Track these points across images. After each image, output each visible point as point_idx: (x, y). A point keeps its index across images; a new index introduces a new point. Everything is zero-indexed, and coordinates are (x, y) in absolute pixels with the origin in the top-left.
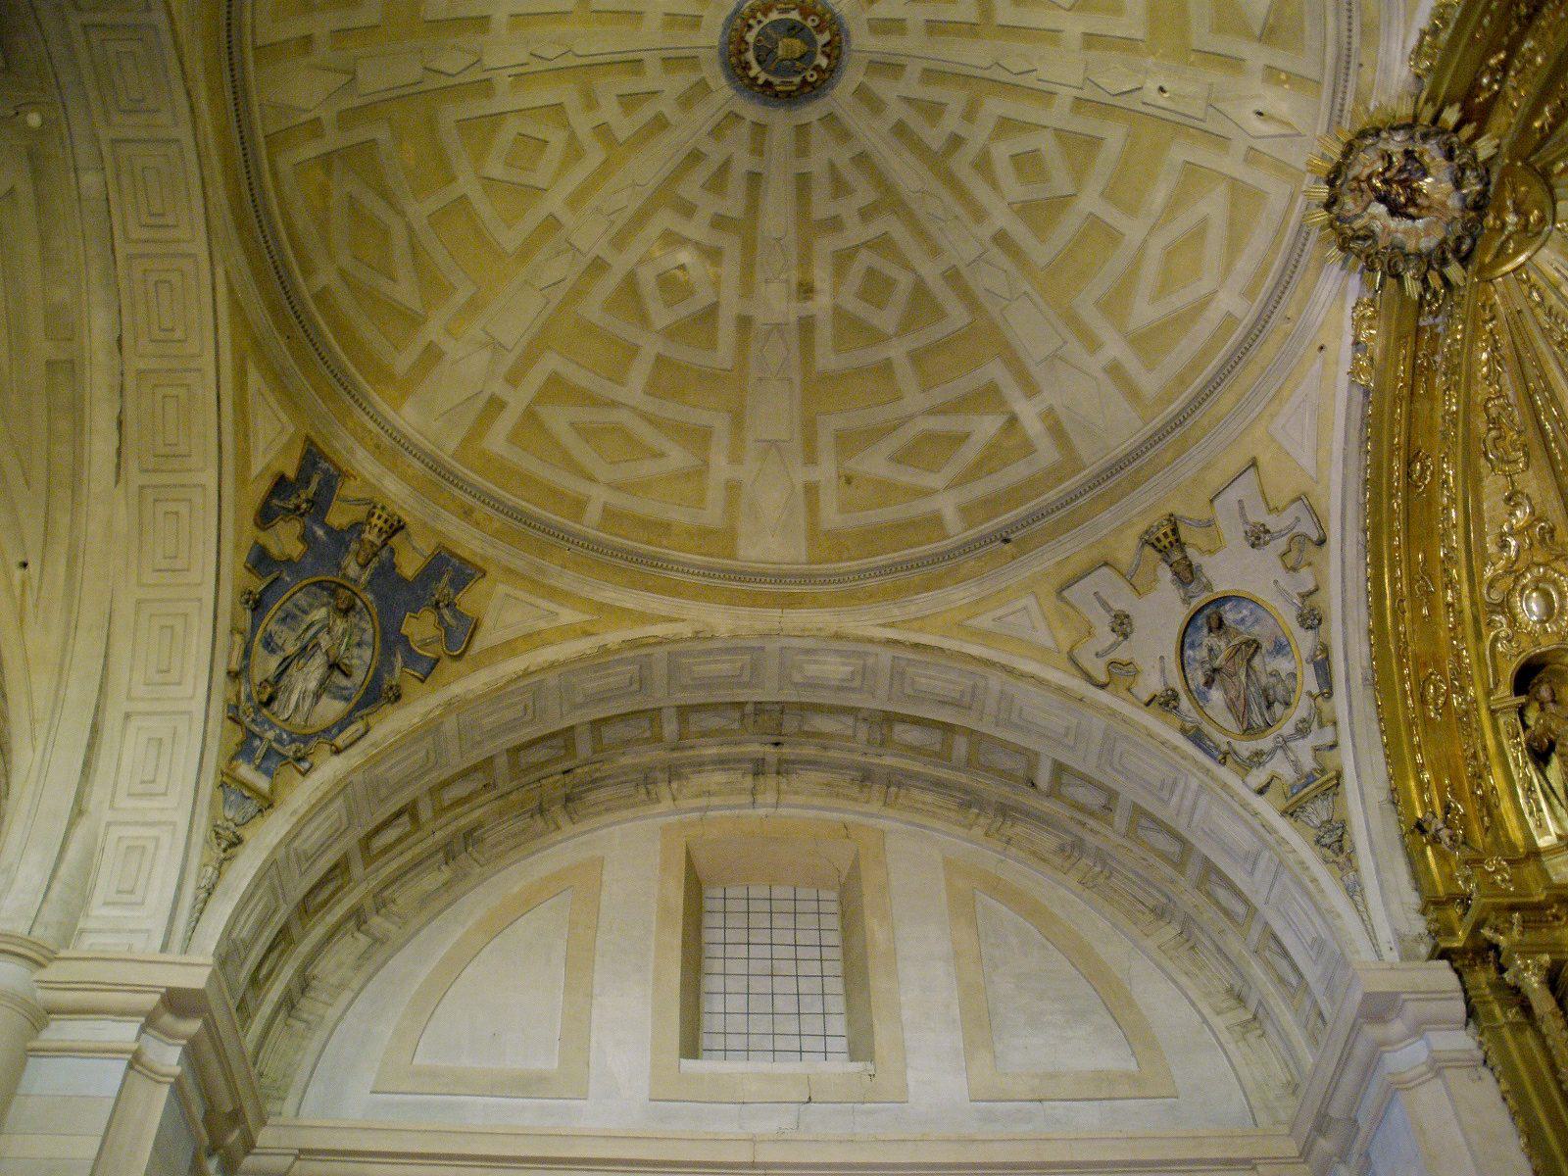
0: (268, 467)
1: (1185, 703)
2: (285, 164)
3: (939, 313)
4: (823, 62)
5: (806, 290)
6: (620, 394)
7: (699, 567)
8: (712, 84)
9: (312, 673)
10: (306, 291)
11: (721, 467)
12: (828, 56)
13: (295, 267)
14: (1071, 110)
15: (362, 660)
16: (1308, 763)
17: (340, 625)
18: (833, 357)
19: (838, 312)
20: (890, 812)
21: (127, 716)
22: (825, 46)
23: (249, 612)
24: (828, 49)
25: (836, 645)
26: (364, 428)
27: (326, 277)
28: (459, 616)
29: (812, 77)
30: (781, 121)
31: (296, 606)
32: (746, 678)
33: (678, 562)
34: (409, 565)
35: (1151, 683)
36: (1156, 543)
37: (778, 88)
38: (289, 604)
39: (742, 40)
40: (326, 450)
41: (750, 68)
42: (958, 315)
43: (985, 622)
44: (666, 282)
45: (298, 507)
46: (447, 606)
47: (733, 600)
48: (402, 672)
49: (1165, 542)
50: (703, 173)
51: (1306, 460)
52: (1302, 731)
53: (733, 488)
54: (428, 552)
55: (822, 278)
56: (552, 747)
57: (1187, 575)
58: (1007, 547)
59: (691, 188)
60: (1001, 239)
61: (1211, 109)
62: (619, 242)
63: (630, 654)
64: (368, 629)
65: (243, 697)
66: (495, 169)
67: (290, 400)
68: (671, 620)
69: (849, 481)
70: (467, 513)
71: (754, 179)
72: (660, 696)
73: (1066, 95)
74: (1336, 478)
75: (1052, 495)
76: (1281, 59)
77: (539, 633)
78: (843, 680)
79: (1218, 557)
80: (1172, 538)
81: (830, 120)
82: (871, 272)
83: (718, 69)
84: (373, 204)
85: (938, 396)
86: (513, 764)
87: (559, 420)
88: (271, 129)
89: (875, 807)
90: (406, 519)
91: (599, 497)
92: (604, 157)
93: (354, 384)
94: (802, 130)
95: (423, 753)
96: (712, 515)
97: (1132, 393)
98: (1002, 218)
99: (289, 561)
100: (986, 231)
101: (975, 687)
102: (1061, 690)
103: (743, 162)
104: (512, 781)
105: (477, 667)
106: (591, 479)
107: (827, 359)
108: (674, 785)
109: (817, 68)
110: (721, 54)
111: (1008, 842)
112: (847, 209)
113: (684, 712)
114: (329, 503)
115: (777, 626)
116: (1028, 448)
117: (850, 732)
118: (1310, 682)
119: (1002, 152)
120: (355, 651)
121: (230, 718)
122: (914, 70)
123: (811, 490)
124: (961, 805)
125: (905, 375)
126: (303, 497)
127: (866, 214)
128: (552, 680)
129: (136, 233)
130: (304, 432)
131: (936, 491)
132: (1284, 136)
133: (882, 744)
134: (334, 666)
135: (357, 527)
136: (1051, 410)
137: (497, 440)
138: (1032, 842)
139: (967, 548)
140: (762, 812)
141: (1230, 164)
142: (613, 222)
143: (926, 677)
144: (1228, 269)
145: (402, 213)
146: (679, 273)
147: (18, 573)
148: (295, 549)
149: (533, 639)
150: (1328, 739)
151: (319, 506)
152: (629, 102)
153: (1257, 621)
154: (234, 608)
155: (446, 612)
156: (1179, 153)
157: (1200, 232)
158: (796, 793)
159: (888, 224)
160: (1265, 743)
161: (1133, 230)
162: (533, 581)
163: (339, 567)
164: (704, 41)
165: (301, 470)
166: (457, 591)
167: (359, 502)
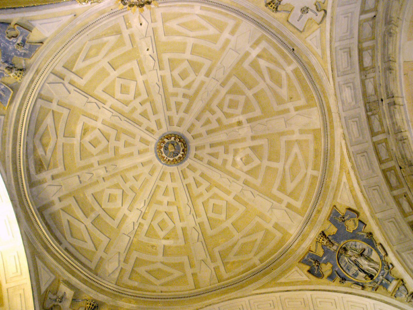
0: (306, 275)
2: (226, 276)
3: (235, 85)
4: (173, 139)
5: (240, 123)
6: (281, 169)
7: (325, 139)
8: (188, 164)
9: (364, 263)
11: (296, 136)
12: (171, 137)
13: (253, 270)
14: (164, 70)
15: (361, 245)
17: (349, 253)
18: (257, 111)
19: (243, 113)
20: (397, 60)
22: (168, 139)
23: (346, 282)
24: (169, 138)
25: (338, 95)
27: (256, 260)
29: (178, 140)
30: (193, 144)
31: (345, 266)
32: (357, 119)
33: (325, 146)
34: (333, 230)
36: (275, 8)
37: (184, 148)
38: (344, 268)
39: (173, 161)
40: (302, 256)
41: (180, 157)
43: (319, 51)
44: (246, 163)
45: (318, 266)
46: (344, 218)
47: (332, 127)
48: (363, 232)
49: (274, 6)
50: (213, 160)
53: (301, 132)
54: (330, 223)
55: (234, 120)
56: (390, 176)
58: (295, 49)
59: (219, 162)
60: (207, 75)
61: (147, 36)
62: (237, 178)
63: (353, 158)
64: (351, 243)
66: (223, 217)
67: (289, 268)
68: (341, 147)
69: (291, 98)
70: (319, 212)
71: (212, 146)
72: (369, 146)
73: (160, 73)
75: (275, 41)
76: (123, 26)
77: (350, 188)
78: (351, 89)
80: (272, 4)
81: (189, 131)
82: (229, 107)
83: (183, 164)
84: (236, 248)
85: (258, 78)
86: (396, 188)
87: (290, 186)
89: (396, 65)
90: (320, 232)
91: (310, 172)
92: (215, 187)
94: (194, 137)
95: (389, 224)
96: (310, 137)
97: (236, 26)
98: (201, 77)
99: (332, 268)
100: (207, 79)
101: (341, 49)
102: (331, 24)
103: (208, 150)
104: (404, 187)
105: (361, 207)
106: (306, 174)
107: (258, 112)
108: (402, 130)
109: (175, 139)
110: (178, 165)
111: (398, 18)
112: (213, 118)
113: (373, 134)
114: (316, 255)
115: (337, 114)
116: (264, 50)
117: (372, 80)
119: (182, 83)
120: (358, 247)
121: (376, 290)
122: (169, 114)
123: (297, 109)
124: (391, 36)
125: (256, 90)
126: (314, 264)
127: (213, 113)
128: (363, 183)
130: (298, 264)
131: (286, 73)
132: (143, 17)
133: (374, 68)
134: (361, 255)
135: (323, 247)
136: (251, 47)
137: (298, 204)
138: (397, 11)
139: (299, 61)
140: (405, 102)
141: (159, 25)
142: (233, 181)
143: (342, 64)
144: (187, 14)
145: (238, 240)
146: (243, 159)
148: (329, 265)
149: (352, 190)
151: (317, 260)
152: (198, 185)
154: (344, 286)
156: (163, 38)
158: (397, 91)
159: (214, 106)
161: (190, 42)
162: (336, 190)
163: (334, 252)
166: (340, 215)
167: (316, 246)
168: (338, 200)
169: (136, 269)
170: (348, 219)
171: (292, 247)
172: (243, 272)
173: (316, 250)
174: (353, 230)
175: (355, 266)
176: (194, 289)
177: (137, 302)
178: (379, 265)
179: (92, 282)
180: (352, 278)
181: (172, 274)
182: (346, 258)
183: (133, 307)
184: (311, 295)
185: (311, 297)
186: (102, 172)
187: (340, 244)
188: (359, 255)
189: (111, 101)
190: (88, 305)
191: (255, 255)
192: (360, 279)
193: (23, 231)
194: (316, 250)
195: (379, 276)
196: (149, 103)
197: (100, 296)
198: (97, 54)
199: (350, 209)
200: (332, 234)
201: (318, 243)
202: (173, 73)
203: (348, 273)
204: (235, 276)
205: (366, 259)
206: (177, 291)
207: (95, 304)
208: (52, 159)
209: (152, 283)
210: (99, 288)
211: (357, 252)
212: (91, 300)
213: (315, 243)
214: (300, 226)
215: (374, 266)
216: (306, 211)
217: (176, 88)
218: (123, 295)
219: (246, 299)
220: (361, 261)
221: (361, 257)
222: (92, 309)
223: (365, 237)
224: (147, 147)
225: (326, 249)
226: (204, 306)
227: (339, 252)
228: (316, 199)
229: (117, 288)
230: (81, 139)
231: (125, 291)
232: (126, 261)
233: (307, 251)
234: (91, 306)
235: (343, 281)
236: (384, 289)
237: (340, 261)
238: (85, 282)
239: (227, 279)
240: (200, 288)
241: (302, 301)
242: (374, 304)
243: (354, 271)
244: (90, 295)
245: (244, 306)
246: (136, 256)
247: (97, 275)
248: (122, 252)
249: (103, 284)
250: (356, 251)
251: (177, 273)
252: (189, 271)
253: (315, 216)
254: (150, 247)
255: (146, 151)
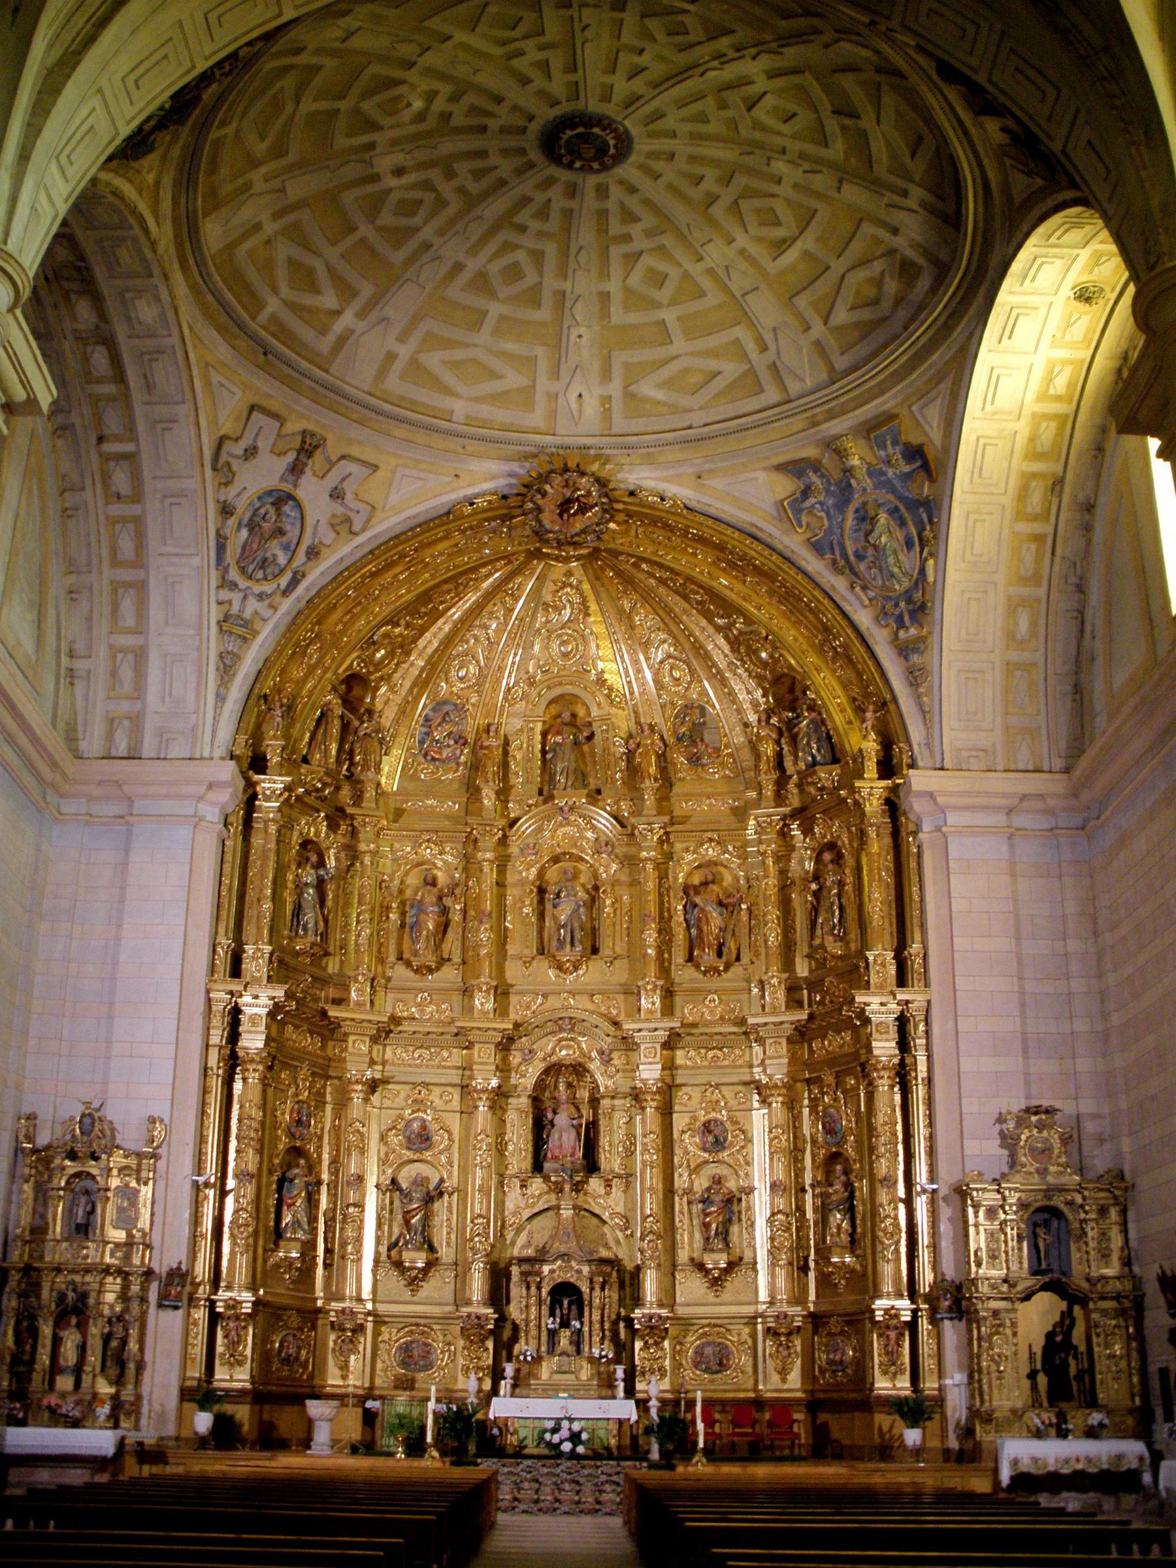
1: (232, 522)
16: (247, 614)
35: (230, 494)
42: (398, 257)
43: (215, 377)
51: (393, 498)
52: (261, 597)
55: (411, 178)
57: (296, 469)
58: (262, 357)
74: (394, 520)
76: (617, 405)
79: (314, 479)
116: (324, 331)
118: (284, 581)
119: (521, 256)
123: (257, 227)
126: (397, 630)
127: (462, 191)
141: (543, 384)
144: (477, 400)
150: (266, 616)
153: (293, 524)
157: (495, 375)
160: (243, 583)
161: (484, 336)
164: (591, 102)
186: (780, 166)
189: (696, 270)
193: (1011, 250)
196: (611, 233)
198: (686, 370)
202: (537, 279)
208: (878, 254)
217: (538, 247)
224: (649, 162)
230: (795, 240)
255: (651, 155)
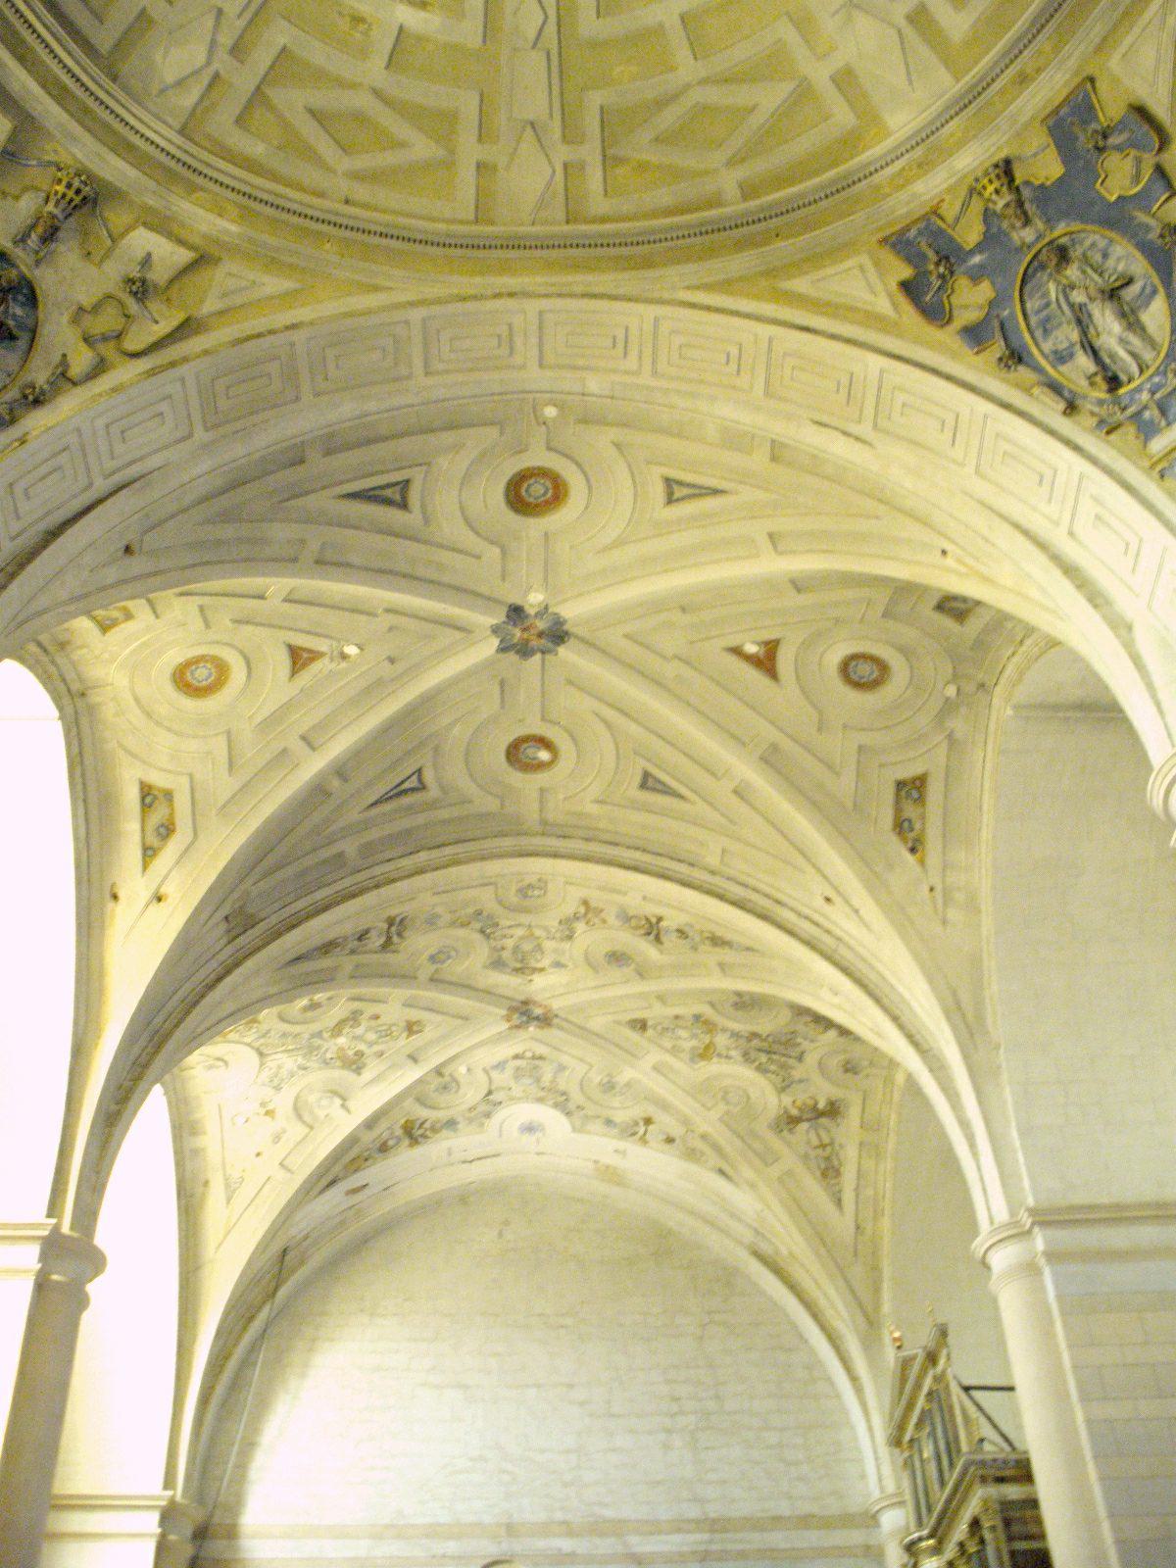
0: (890, 296)
2: (598, 204)
9: (1108, 326)
10: (735, 208)
17: (1072, 272)
21: (1071, 534)
23: (1021, 368)
26: (892, 178)
28: (1121, 125)
31: (1038, 312)
34: (1047, 168)
38: (1033, 320)
40: (896, 228)
45: (942, 277)
46: (1105, 137)
48: (1153, 216)
64: (1094, 237)
65: (1096, 409)
70: (1023, 79)
84: (669, 117)
88: (561, 215)
90: (1003, 154)
93: (849, 173)
99: (992, 304)
114: (951, 240)
120: (1111, 263)
121: (1108, 433)
126: (931, 267)
129: (632, 363)
134: (1112, 294)
135: (988, 215)
145: (688, 86)
147: (949, 561)
148: (985, 291)
151: (950, 256)
155: (1113, 140)
163: (1019, 250)
165: (908, 260)
166: (1096, 117)
167: (965, 206)
168: (1114, 63)
169: (269, 92)
170: (1119, 148)
171: (877, 178)
172: (669, 212)
173: (957, 220)
174: (1119, 197)
175: (1073, 325)
176: (467, 222)
177: (245, 215)
178: (1159, 353)
179: (90, 102)
180: (1044, 363)
181: (402, 145)
182: (1052, 287)
183: (226, 232)
184: (882, 372)
185: (881, 381)
187: (1052, 230)
188: (1103, 292)
190: (58, 188)
191: (730, 163)
192: (1073, 376)
194: (957, 220)
195: (1139, 389)
197: (113, 162)
199: (1141, 112)
200: (1037, 183)
201: (975, 197)
203: (1040, 339)
204: (634, 217)
205: (1123, 315)
206: (410, 215)
207: (87, 189)
209: (318, 161)
210: (114, 132)
211: (1100, 281)
212: (72, 171)
213: (963, 192)
214: (934, 108)
215: (1137, 351)
216: (980, 59)
218: (200, 180)
219: (650, 312)
220: (1103, 315)
221: (1108, 304)
222: (73, 204)
223: (1153, 236)
225: (994, 230)
226: (489, 292)
227: (1035, 256)
228: (1033, 22)
229: (179, 147)
231: (209, 165)
232: (238, 50)
233: (922, 212)
234: (71, 194)
235: (1010, 363)
236: (1137, 438)
237: (1028, 288)
238: (61, 95)
239: (603, 220)
240: (492, 223)
241: (845, 381)
242: (1081, 477)
243: (1061, 342)
244: (75, 151)
245: (634, 332)
246: (282, 40)
247: (114, 79)
248: (231, 10)
249: (132, 121)
250: (1101, 274)
251: (422, 148)
252: (469, 150)
253: (1002, 91)
254: (348, 19)
